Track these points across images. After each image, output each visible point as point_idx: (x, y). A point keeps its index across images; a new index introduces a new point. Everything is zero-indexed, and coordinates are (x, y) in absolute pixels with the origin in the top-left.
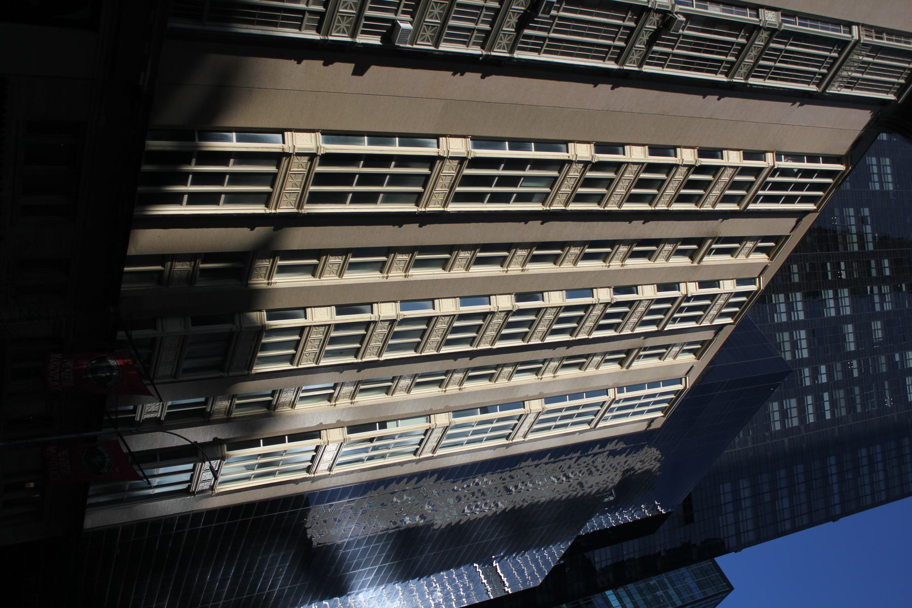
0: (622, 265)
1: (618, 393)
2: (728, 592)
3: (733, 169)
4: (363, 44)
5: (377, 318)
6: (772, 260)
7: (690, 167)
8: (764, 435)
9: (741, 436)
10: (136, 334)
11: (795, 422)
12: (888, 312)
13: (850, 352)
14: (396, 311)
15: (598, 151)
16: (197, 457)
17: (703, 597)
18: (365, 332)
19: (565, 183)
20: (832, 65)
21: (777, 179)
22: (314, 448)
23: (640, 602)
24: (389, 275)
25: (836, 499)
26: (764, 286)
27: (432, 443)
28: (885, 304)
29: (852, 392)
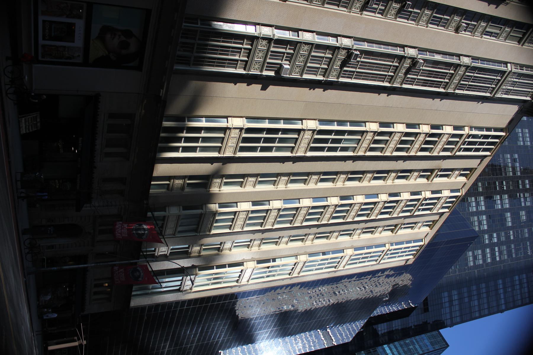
6: (468, 180)
7: (426, 134)
8: (465, 268)
9: (453, 268)
10: (156, 214)
11: (481, 262)
12: (529, 206)
13: (509, 226)
16: (203, 210)
20: (498, 83)
21: (470, 140)
23: (401, 351)
25: (503, 301)
29: (510, 247)
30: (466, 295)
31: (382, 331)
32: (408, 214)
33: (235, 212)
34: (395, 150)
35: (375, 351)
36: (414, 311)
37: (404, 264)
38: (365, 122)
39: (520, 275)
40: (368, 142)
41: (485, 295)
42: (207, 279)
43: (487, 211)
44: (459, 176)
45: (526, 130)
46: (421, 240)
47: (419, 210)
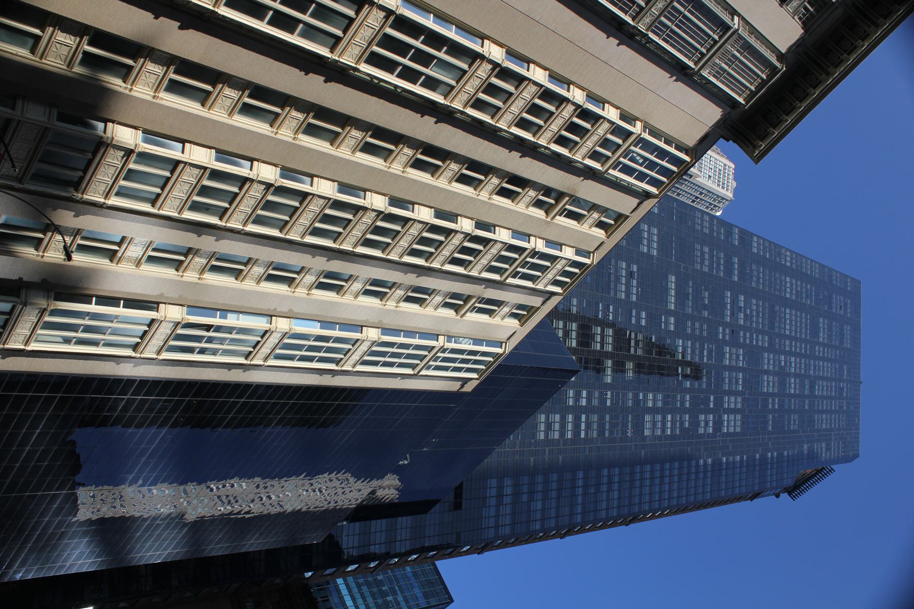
0: (396, 307)
1: (447, 342)
2: (449, 604)
3: (502, 245)
4: (223, 16)
5: (255, 176)
6: (608, 238)
7: (467, 235)
8: (531, 441)
9: (511, 439)
11: (557, 436)
12: (639, 357)
13: (607, 383)
14: (276, 176)
15: (391, 204)
16: (19, 298)
17: (427, 606)
18: (228, 206)
19: (483, 66)
20: (712, 46)
21: (535, 261)
22: (140, 334)
23: (372, 605)
24: (185, 274)
25: (579, 509)
26: (597, 262)
27: (265, 350)
28: (638, 349)
30: (525, 489)
31: (377, 533)
32: (409, 371)
33: (177, 163)
34: (416, 241)
35: (326, 601)
36: (438, 505)
37: (456, 390)
38: (365, 190)
39: (611, 469)
40: (364, 227)
41: (554, 494)
42: (62, 337)
43: (578, 349)
44: (509, 316)
45: (623, 263)
46: (499, 344)
47: (428, 368)
